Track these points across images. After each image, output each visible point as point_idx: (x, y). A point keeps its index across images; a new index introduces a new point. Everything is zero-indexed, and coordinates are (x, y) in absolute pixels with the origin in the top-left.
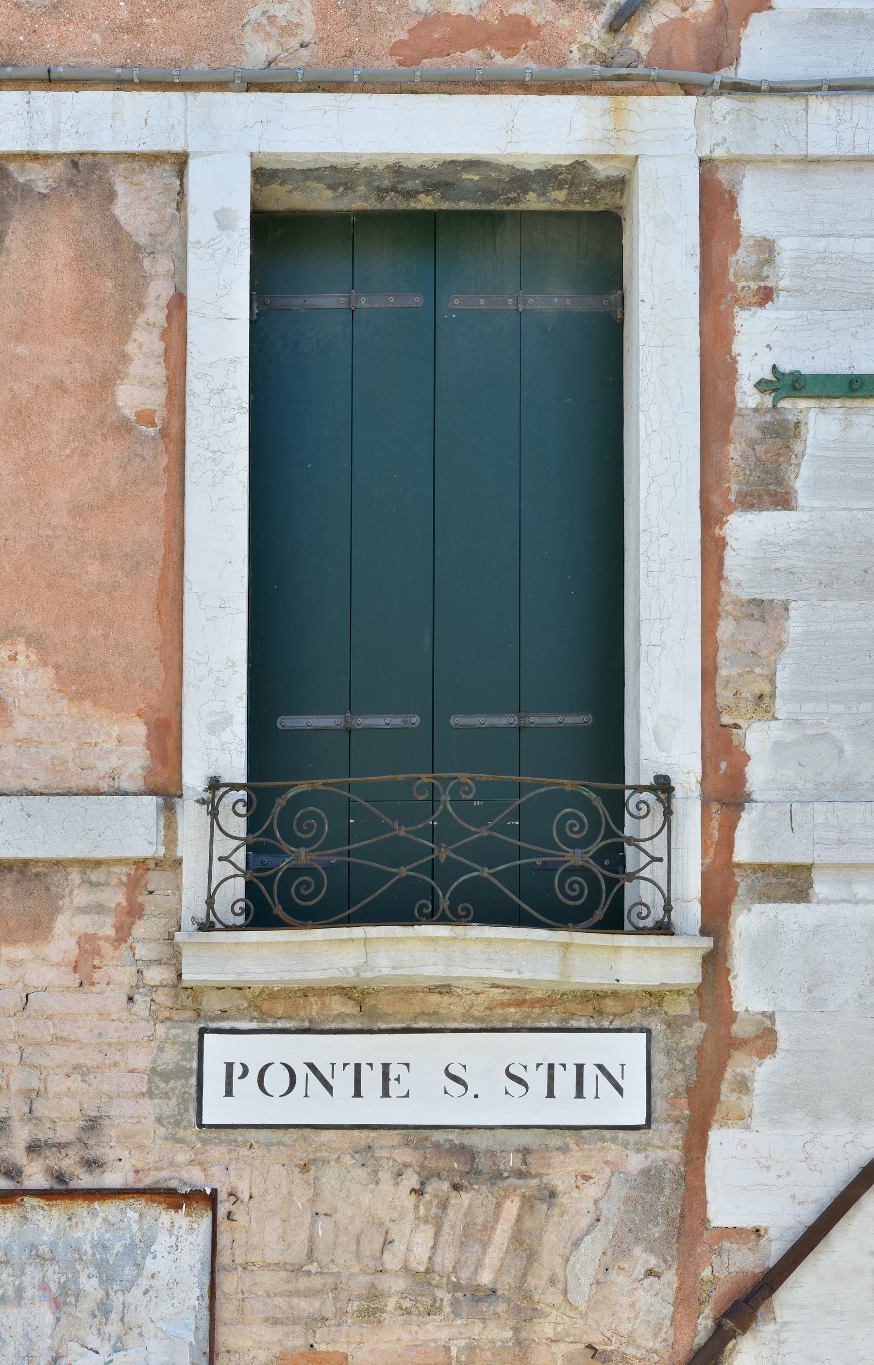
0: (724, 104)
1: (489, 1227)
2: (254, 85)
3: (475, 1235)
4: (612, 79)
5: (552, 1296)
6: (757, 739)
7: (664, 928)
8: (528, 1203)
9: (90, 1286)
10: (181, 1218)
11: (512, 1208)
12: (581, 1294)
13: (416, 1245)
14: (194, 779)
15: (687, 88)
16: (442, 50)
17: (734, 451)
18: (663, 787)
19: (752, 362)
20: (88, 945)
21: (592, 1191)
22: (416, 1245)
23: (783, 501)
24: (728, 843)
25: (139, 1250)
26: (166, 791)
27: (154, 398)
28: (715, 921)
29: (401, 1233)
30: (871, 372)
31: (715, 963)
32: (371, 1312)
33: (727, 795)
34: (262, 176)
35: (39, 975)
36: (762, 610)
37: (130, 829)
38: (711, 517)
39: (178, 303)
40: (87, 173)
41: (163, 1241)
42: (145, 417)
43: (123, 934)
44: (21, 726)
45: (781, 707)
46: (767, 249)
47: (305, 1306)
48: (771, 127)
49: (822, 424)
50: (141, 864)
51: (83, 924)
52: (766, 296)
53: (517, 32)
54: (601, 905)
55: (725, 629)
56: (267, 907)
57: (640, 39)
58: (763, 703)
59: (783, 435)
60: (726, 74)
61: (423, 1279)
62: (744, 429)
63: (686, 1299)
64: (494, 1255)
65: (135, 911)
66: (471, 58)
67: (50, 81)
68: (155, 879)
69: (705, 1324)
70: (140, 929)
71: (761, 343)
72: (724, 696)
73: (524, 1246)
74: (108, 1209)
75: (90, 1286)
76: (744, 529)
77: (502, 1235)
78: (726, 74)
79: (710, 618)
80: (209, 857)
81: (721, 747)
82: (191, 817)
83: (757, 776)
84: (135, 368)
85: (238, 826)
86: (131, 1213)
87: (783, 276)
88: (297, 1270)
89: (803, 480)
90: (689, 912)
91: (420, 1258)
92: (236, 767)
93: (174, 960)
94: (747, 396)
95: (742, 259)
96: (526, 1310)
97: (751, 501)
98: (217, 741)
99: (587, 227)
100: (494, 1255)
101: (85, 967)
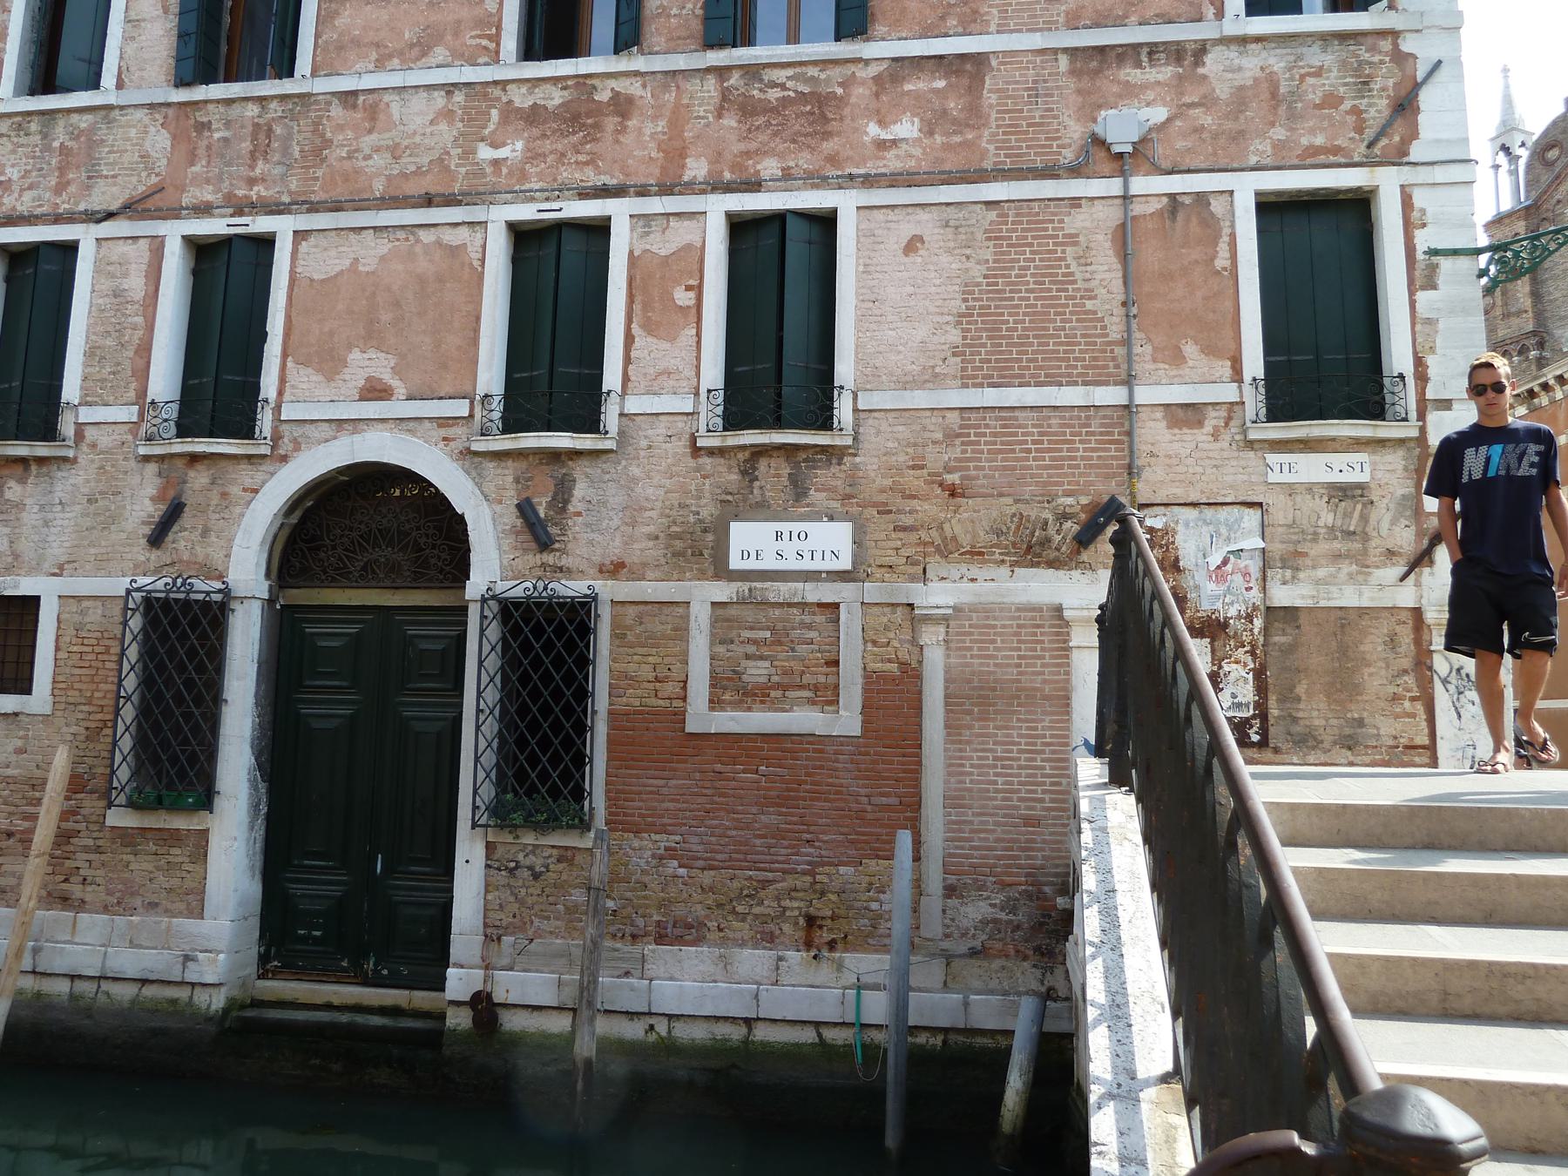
0: (1406, 168)
1: (1352, 513)
2: (1253, 169)
3: (1347, 515)
4: (1369, 163)
5: (1375, 534)
6: (1431, 361)
7: (1405, 420)
8: (1364, 505)
9: (1223, 530)
10: (1251, 511)
11: (1359, 507)
12: (1384, 532)
13: (1328, 518)
14: (1247, 378)
15: (1394, 164)
16: (1314, 155)
17: (1417, 273)
18: (1401, 377)
19: (1421, 247)
20: (1216, 428)
21: (1385, 501)
22: (1328, 518)
23: (1434, 287)
24: (1424, 393)
25: (1239, 520)
26: (1237, 376)
27: (1227, 263)
28: (1421, 416)
29: (1323, 514)
30: (27, 4)
31: (1423, 430)
32: (1315, 539)
33: (1422, 377)
34: (1258, 194)
35: (1201, 438)
36: (1429, 322)
37: (1229, 393)
38: (1412, 293)
39: (1233, 236)
40: (1201, 198)
41: (1246, 518)
42: (1225, 269)
43: (1227, 424)
44: (1191, 363)
45: (1438, 350)
46: (1423, 211)
47: (1295, 538)
48: (1423, 175)
49: (1445, 264)
50: (1231, 403)
51: (1214, 422)
52: (1424, 225)
53: (1336, 150)
54: (1376, 410)
55: (1418, 327)
56: (1273, 416)
57: (1377, 150)
58: (1432, 350)
59: (1433, 269)
60: (1405, 159)
61: (1332, 529)
62: (1420, 266)
63: (1420, 534)
64: (1354, 522)
65: (1229, 419)
66: (1322, 158)
67: (1189, 171)
68: (1236, 408)
69: (1426, 542)
70: (1232, 423)
71: (1423, 240)
72: (1419, 348)
73: (1364, 519)
74: (1228, 508)
75: (1223, 530)
76: (1422, 297)
77: (1356, 514)
78: (1405, 159)
79: (1413, 324)
80: (1254, 402)
81: (1419, 362)
82: (1248, 391)
83: (1431, 372)
84: (1221, 254)
85: (1262, 391)
86: (1236, 509)
87: (1429, 218)
88: (1289, 526)
89: (1440, 281)
90: (1413, 415)
91: (1330, 521)
92: (1261, 374)
93: (1245, 432)
94: (1420, 256)
95: (1415, 214)
96: (1366, 538)
97: (1423, 288)
98: (1254, 362)
99: (1359, 205)
100: (1354, 522)
101: (1215, 436)
